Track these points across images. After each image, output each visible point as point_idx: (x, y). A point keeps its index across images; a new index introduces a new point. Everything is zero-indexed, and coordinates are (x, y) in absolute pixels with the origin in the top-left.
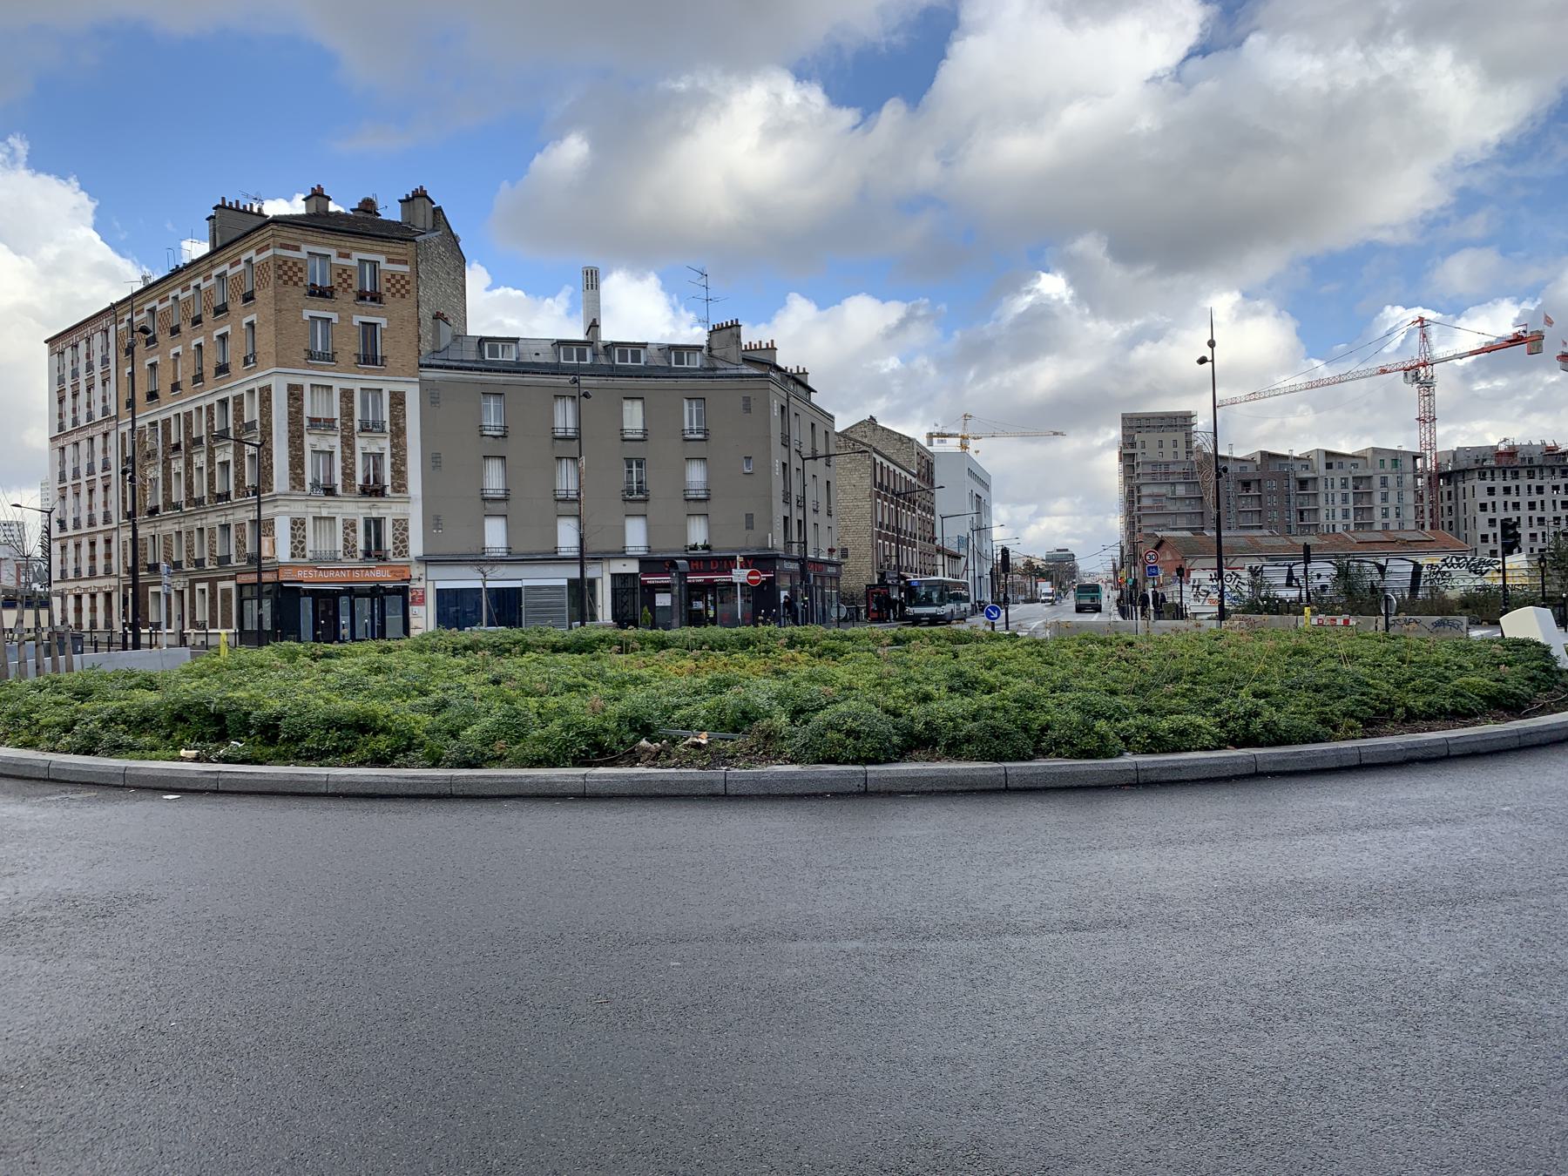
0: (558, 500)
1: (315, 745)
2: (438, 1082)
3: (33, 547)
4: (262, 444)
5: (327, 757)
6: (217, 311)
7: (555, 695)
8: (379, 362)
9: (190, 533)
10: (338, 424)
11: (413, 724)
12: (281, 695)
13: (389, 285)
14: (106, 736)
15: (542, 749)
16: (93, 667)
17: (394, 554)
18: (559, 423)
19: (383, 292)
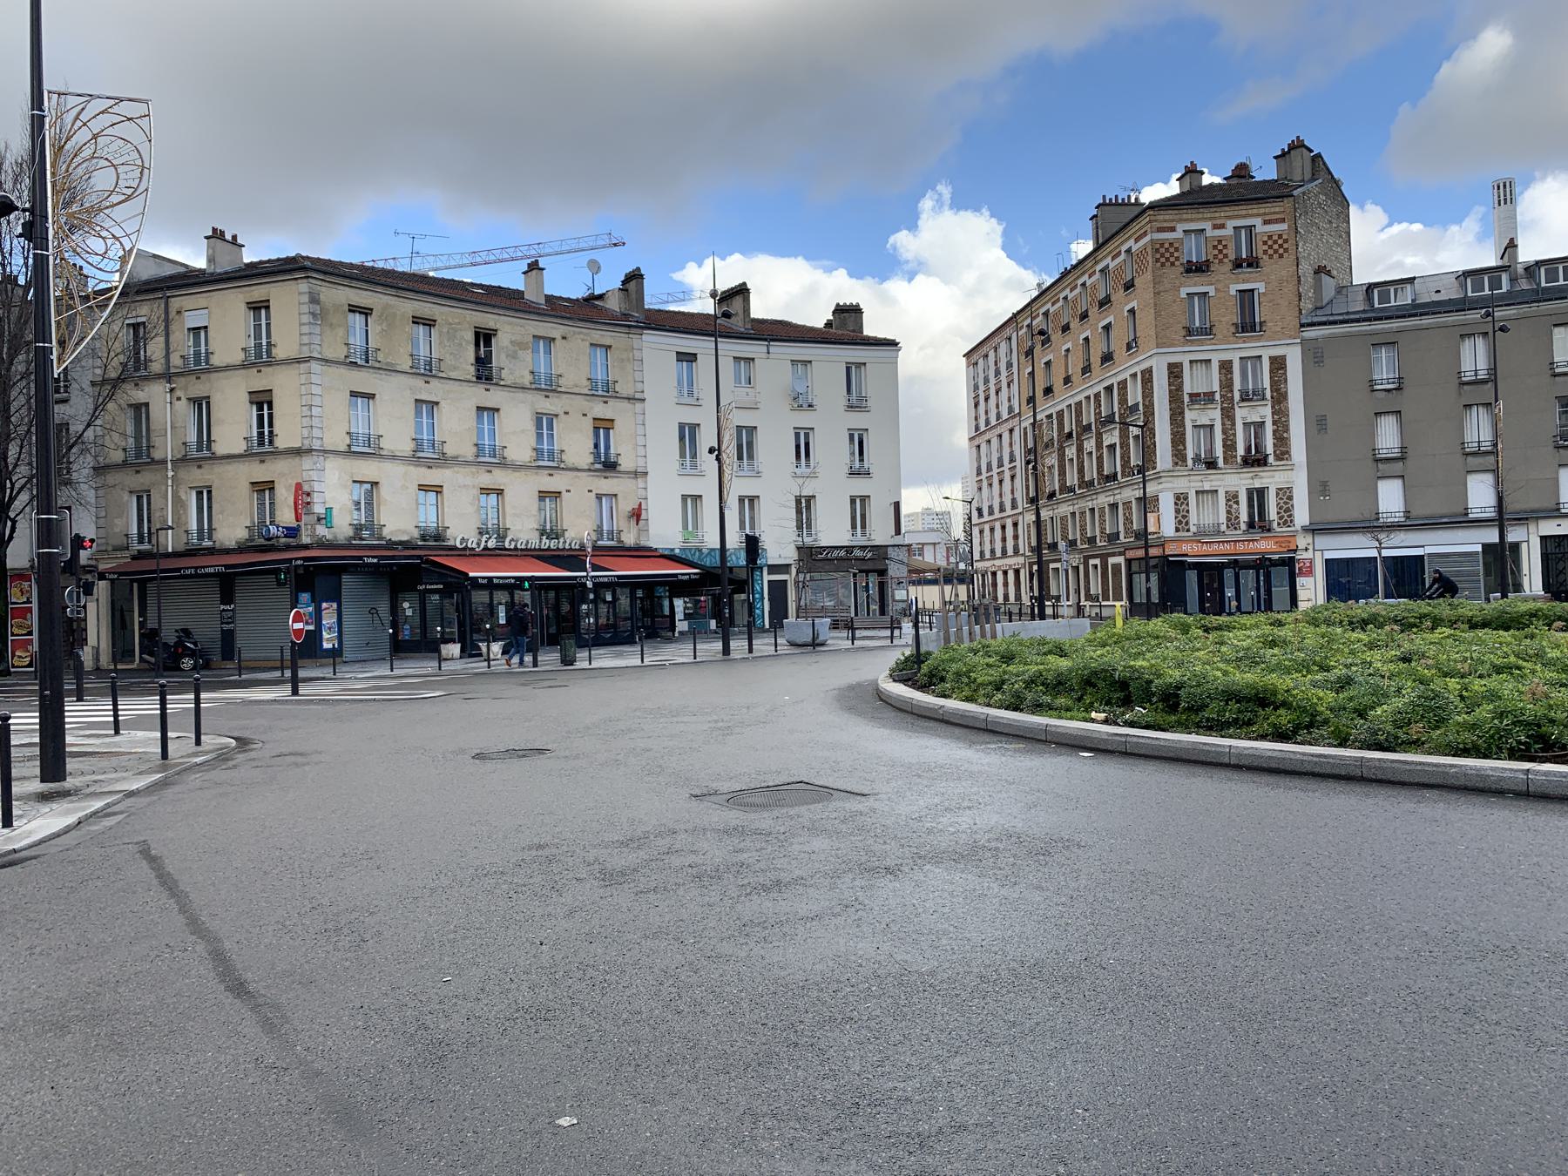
0: (1468, 454)
1: (1215, 716)
2: (1378, 1079)
3: (958, 532)
4: (1145, 424)
5: (1228, 728)
6: (1101, 304)
7: (1481, 677)
8: (1258, 329)
9: (1083, 513)
10: (1217, 396)
11: (1315, 701)
12: (1179, 665)
13: (1266, 247)
14: (1029, 696)
15: (1468, 737)
16: (1014, 635)
17: (1279, 524)
18: (1467, 366)
19: (1260, 256)
